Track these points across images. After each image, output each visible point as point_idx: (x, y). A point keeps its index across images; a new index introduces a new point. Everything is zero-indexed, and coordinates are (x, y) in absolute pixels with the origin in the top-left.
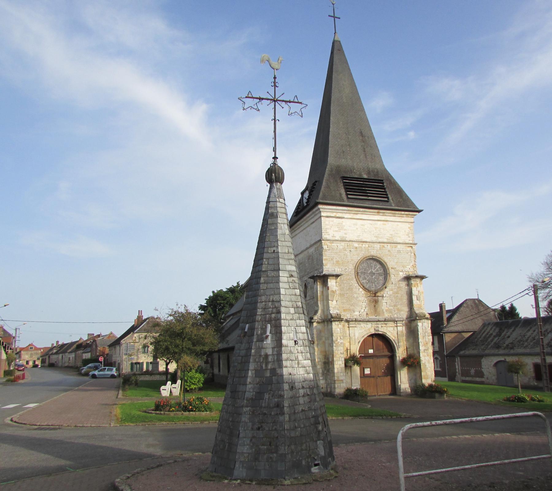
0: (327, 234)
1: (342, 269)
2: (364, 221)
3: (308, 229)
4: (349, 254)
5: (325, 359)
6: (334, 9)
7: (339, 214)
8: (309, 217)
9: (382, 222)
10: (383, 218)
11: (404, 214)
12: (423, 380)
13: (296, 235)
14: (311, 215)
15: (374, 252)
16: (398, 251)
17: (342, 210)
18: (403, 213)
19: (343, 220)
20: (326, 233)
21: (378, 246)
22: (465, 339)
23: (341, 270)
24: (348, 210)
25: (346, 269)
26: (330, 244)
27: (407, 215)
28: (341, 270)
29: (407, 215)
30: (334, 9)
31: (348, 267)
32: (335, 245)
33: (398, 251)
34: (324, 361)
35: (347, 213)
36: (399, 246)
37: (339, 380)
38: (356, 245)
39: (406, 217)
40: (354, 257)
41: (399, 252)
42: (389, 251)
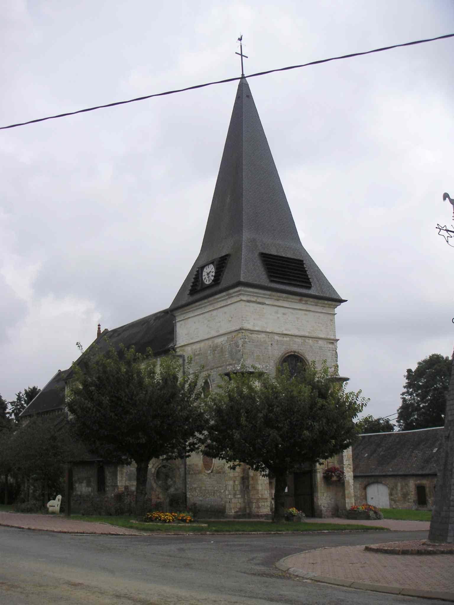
0: (247, 322)
1: (263, 366)
2: (286, 309)
3: (214, 313)
4: (270, 348)
5: (244, 473)
6: (241, 46)
7: (259, 298)
8: (218, 298)
9: (303, 312)
10: (304, 307)
11: (326, 304)
12: (346, 499)
13: (189, 318)
14: (224, 296)
15: (296, 346)
16: (319, 347)
17: (253, 292)
18: (326, 302)
19: (264, 306)
20: (247, 321)
21: (299, 340)
22: (41, 392)
23: (262, 367)
24: (264, 294)
25: (267, 366)
26: (250, 335)
27: (329, 305)
28: (262, 367)
29: (329, 305)
30: (241, 46)
31: (269, 364)
32: (254, 336)
33: (319, 347)
34: (242, 475)
35: (268, 298)
36: (321, 342)
37: (263, 499)
38: (277, 337)
39: (328, 307)
40: (276, 351)
41: (321, 348)
42: (311, 346)
